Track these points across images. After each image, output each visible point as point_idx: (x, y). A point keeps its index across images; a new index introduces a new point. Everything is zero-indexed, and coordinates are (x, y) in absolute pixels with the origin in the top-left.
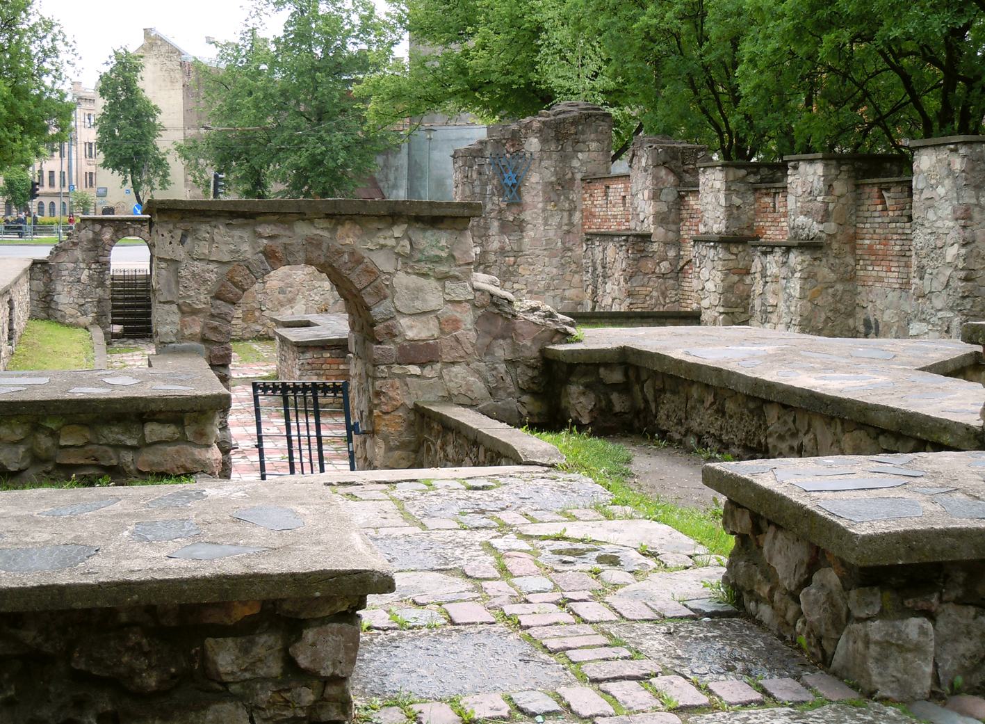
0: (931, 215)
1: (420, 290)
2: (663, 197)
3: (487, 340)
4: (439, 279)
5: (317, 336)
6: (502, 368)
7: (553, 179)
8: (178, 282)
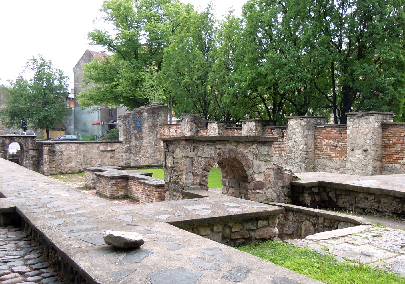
0: (294, 137)
1: (260, 165)
2: (193, 131)
3: (277, 180)
4: (265, 162)
5: (115, 174)
6: (280, 189)
7: (152, 125)
8: (192, 165)
